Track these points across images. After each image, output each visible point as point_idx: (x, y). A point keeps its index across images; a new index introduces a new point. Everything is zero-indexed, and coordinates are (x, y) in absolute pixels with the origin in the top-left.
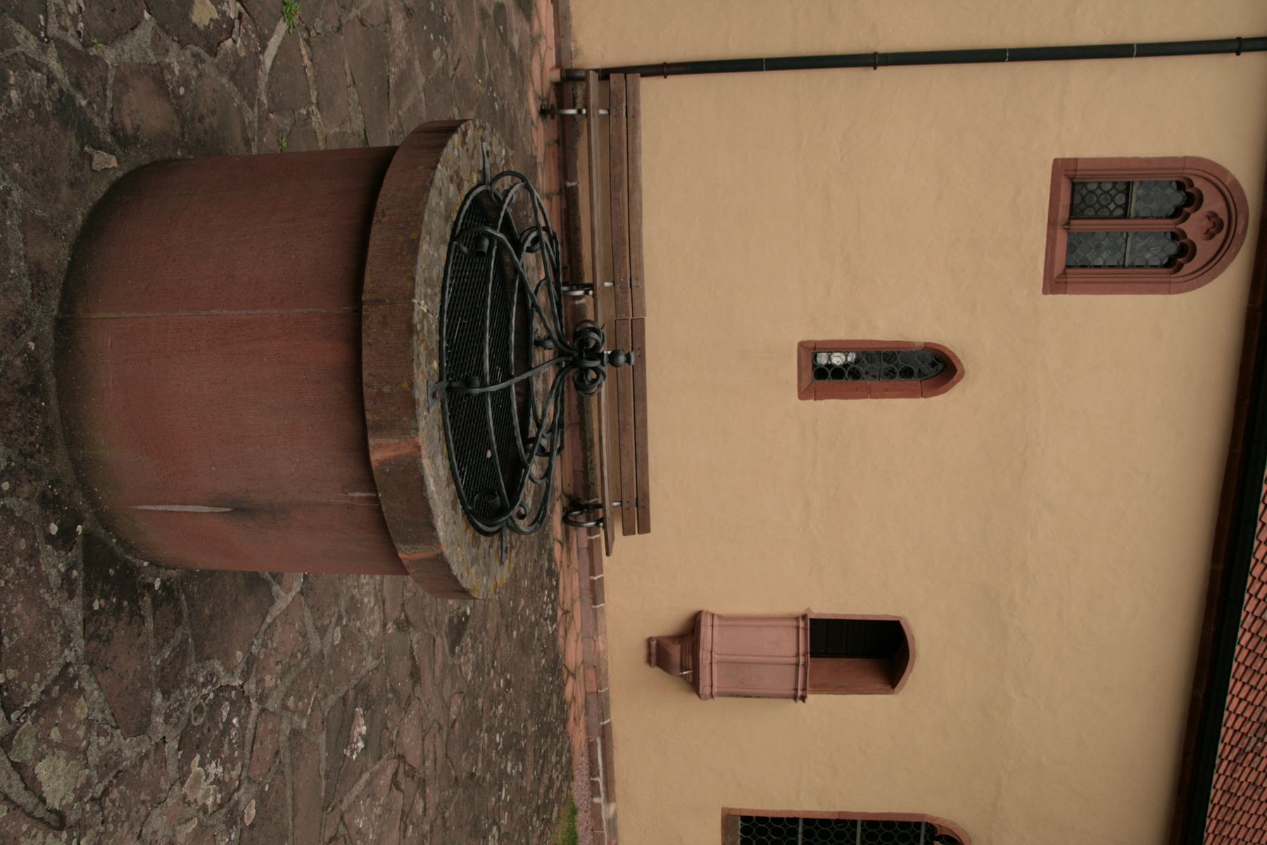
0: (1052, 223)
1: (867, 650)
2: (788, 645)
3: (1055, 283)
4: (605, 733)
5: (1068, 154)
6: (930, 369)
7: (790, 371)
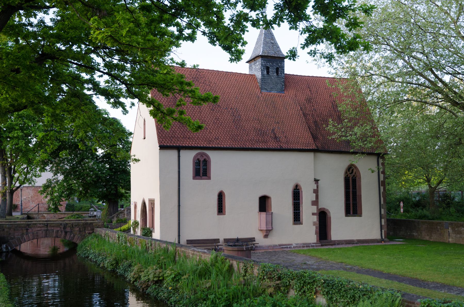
0: (201, 179)
1: (264, 203)
2: (263, 214)
3: (209, 178)
4: (280, 245)
5: (192, 178)
6: (221, 196)
7: (221, 216)
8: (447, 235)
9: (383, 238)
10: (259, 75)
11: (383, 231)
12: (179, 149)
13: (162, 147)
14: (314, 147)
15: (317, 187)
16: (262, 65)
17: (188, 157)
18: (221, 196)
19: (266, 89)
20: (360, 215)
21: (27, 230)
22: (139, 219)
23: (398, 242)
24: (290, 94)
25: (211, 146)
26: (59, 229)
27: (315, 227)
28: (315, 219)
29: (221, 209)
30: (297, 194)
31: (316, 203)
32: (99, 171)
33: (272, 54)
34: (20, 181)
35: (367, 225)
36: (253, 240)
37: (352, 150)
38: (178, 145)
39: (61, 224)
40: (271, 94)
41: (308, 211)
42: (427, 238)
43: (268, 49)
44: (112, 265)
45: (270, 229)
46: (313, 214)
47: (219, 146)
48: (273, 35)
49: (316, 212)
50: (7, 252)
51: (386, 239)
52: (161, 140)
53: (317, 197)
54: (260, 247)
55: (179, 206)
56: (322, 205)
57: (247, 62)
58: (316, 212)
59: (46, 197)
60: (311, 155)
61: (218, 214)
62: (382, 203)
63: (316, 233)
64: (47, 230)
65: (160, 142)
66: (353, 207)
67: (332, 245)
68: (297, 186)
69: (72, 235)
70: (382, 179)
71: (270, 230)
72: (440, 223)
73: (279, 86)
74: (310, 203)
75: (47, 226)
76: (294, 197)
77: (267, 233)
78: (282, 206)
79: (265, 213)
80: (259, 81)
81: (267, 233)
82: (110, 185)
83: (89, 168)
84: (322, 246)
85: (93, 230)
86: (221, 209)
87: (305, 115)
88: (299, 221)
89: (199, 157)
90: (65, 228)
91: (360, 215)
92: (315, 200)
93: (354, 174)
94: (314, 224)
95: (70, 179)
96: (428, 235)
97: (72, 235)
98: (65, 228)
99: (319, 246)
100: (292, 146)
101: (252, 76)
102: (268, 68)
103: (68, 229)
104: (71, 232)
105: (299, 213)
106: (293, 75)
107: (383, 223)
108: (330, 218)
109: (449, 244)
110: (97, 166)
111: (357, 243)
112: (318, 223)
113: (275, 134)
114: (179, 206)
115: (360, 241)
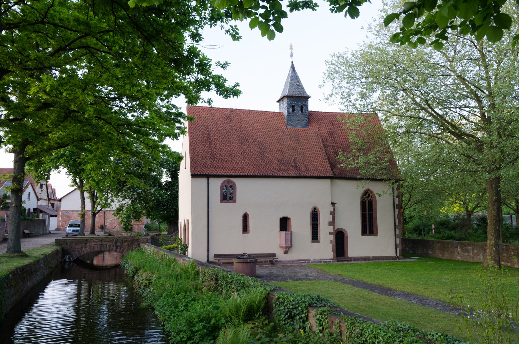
1: (285, 224)
2: (283, 233)
4: (299, 260)
6: (245, 217)
8: (457, 253)
9: (398, 255)
10: (285, 112)
11: (398, 249)
12: (208, 177)
13: (193, 176)
14: (331, 174)
15: (334, 209)
16: (288, 104)
17: (216, 184)
18: (246, 217)
19: (292, 125)
20: (376, 235)
21: (86, 244)
22: (182, 237)
23: (415, 259)
24: (313, 129)
25: (236, 174)
26: (111, 244)
27: (331, 245)
28: (332, 237)
29: (245, 229)
30: (315, 216)
31: (332, 223)
32: (160, 196)
33: (297, 94)
34: (101, 205)
35: (383, 243)
36: (273, 255)
37: (358, 177)
38: (207, 173)
39: (113, 240)
40: (296, 128)
41: (326, 232)
42: (440, 256)
43: (294, 90)
44: (133, 272)
45: (290, 246)
46: (330, 233)
47: (244, 174)
48: (299, 78)
49: (332, 231)
50: (70, 262)
51: (401, 257)
52: (193, 169)
53: (334, 218)
54: (280, 261)
55: (208, 225)
56: (340, 225)
57: (277, 102)
58: (332, 231)
59: (119, 218)
60: (328, 182)
61: (243, 233)
62: (397, 223)
63: (333, 250)
64: (102, 244)
65: (192, 171)
66: (369, 227)
67: (348, 261)
68: (315, 208)
69: (122, 249)
70: (397, 202)
71: (290, 247)
72: (451, 242)
73: (304, 122)
74: (327, 224)
75: (102, 241)
76: (312, 218)
77: (287, 250)
78: (301, 226)
79: (284, 232)
80: (285, 117)
81: (287, 250)
82: (171, 209)
83: (151, 194)
84: (338, 261)
85: (139, 245)
86: (245, 229)
87: (325, 146)
88: (317, 239)
89: (226, 184)
90: (116, 243)
91: (376, 235)
92: (331, 221)
93: (370, 198)
94: (331, 242)
95: (136, 204)
96: (441, 253)
97: (122, 249)
98: (116, 243)
99: (335, 262)
100: (310, 174)
101: (280, 114)
102: (293, 107)
103: (119, 244)
104: (121, 247)
105: (317, 232)
106: (318, 112)
107: (398, 242)
108: (347, 237)
109: (458, 261)
110: (159, 192)
111: (372, 260)
112: (335, 241)
113: (296, 164)
114: (208, 225)
115: (375, 258)
